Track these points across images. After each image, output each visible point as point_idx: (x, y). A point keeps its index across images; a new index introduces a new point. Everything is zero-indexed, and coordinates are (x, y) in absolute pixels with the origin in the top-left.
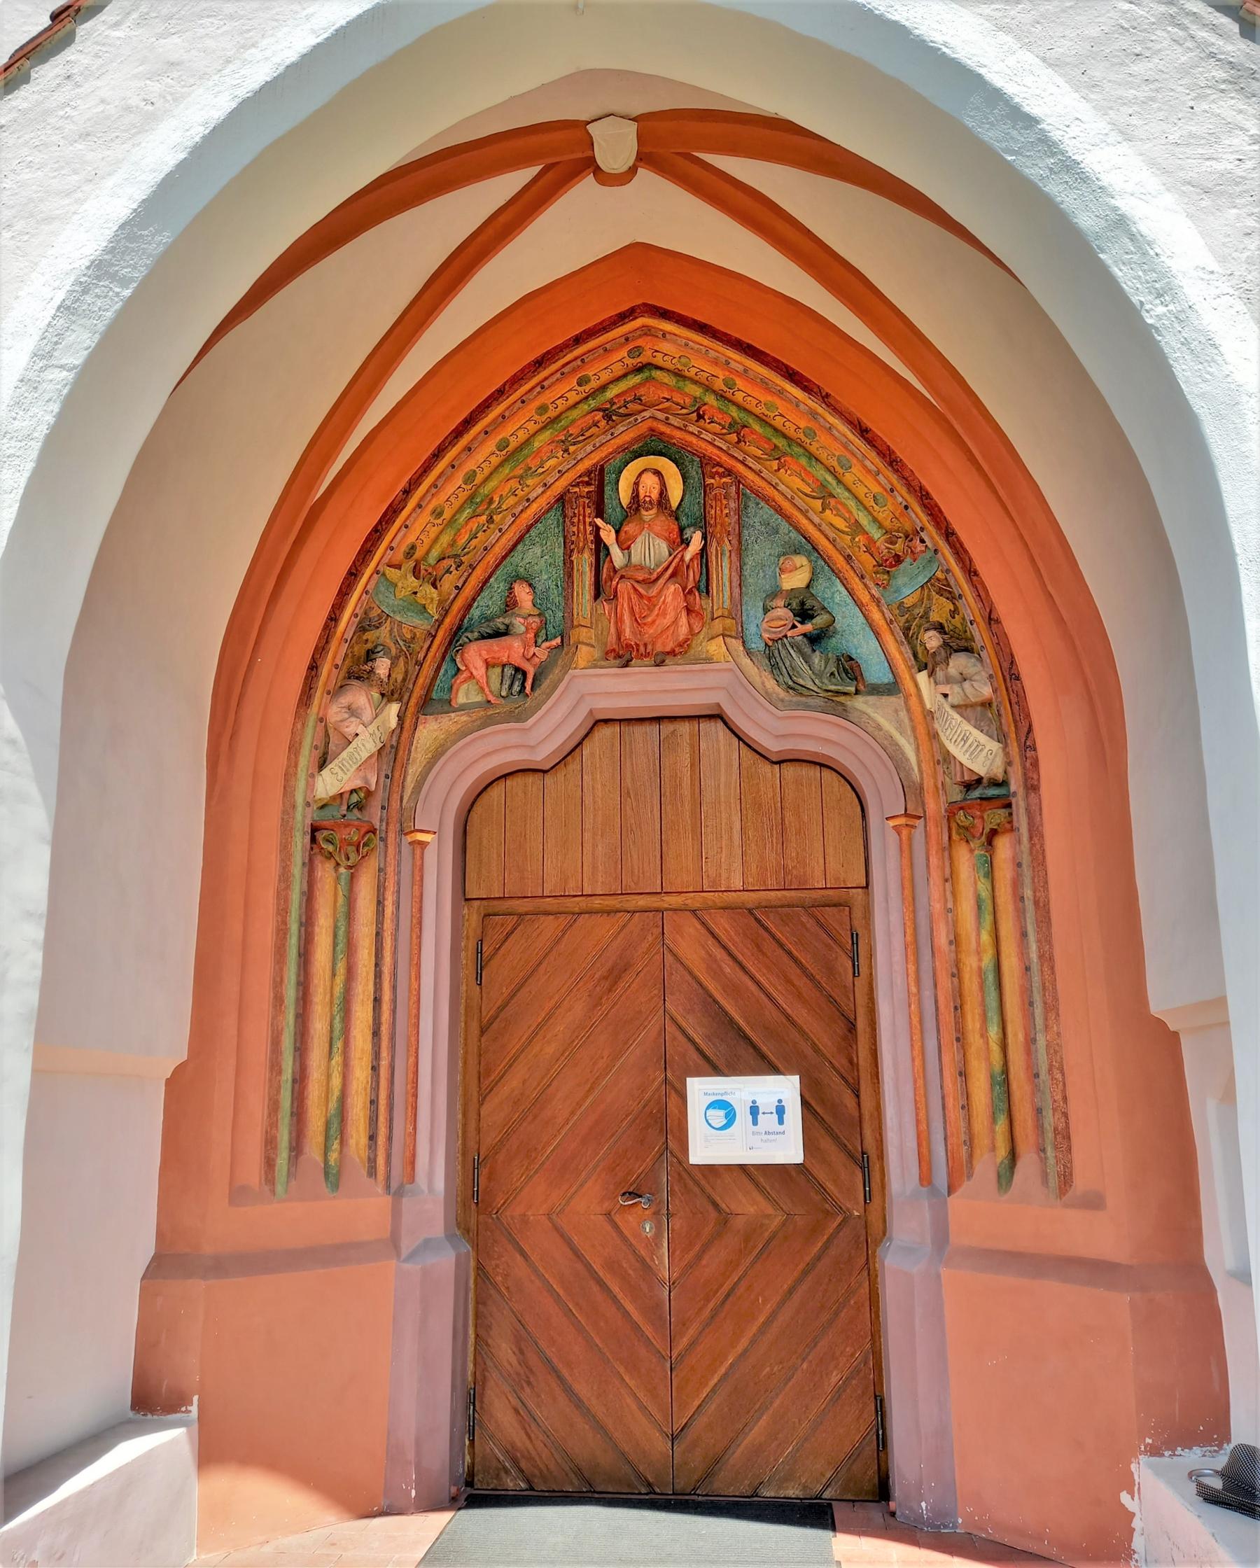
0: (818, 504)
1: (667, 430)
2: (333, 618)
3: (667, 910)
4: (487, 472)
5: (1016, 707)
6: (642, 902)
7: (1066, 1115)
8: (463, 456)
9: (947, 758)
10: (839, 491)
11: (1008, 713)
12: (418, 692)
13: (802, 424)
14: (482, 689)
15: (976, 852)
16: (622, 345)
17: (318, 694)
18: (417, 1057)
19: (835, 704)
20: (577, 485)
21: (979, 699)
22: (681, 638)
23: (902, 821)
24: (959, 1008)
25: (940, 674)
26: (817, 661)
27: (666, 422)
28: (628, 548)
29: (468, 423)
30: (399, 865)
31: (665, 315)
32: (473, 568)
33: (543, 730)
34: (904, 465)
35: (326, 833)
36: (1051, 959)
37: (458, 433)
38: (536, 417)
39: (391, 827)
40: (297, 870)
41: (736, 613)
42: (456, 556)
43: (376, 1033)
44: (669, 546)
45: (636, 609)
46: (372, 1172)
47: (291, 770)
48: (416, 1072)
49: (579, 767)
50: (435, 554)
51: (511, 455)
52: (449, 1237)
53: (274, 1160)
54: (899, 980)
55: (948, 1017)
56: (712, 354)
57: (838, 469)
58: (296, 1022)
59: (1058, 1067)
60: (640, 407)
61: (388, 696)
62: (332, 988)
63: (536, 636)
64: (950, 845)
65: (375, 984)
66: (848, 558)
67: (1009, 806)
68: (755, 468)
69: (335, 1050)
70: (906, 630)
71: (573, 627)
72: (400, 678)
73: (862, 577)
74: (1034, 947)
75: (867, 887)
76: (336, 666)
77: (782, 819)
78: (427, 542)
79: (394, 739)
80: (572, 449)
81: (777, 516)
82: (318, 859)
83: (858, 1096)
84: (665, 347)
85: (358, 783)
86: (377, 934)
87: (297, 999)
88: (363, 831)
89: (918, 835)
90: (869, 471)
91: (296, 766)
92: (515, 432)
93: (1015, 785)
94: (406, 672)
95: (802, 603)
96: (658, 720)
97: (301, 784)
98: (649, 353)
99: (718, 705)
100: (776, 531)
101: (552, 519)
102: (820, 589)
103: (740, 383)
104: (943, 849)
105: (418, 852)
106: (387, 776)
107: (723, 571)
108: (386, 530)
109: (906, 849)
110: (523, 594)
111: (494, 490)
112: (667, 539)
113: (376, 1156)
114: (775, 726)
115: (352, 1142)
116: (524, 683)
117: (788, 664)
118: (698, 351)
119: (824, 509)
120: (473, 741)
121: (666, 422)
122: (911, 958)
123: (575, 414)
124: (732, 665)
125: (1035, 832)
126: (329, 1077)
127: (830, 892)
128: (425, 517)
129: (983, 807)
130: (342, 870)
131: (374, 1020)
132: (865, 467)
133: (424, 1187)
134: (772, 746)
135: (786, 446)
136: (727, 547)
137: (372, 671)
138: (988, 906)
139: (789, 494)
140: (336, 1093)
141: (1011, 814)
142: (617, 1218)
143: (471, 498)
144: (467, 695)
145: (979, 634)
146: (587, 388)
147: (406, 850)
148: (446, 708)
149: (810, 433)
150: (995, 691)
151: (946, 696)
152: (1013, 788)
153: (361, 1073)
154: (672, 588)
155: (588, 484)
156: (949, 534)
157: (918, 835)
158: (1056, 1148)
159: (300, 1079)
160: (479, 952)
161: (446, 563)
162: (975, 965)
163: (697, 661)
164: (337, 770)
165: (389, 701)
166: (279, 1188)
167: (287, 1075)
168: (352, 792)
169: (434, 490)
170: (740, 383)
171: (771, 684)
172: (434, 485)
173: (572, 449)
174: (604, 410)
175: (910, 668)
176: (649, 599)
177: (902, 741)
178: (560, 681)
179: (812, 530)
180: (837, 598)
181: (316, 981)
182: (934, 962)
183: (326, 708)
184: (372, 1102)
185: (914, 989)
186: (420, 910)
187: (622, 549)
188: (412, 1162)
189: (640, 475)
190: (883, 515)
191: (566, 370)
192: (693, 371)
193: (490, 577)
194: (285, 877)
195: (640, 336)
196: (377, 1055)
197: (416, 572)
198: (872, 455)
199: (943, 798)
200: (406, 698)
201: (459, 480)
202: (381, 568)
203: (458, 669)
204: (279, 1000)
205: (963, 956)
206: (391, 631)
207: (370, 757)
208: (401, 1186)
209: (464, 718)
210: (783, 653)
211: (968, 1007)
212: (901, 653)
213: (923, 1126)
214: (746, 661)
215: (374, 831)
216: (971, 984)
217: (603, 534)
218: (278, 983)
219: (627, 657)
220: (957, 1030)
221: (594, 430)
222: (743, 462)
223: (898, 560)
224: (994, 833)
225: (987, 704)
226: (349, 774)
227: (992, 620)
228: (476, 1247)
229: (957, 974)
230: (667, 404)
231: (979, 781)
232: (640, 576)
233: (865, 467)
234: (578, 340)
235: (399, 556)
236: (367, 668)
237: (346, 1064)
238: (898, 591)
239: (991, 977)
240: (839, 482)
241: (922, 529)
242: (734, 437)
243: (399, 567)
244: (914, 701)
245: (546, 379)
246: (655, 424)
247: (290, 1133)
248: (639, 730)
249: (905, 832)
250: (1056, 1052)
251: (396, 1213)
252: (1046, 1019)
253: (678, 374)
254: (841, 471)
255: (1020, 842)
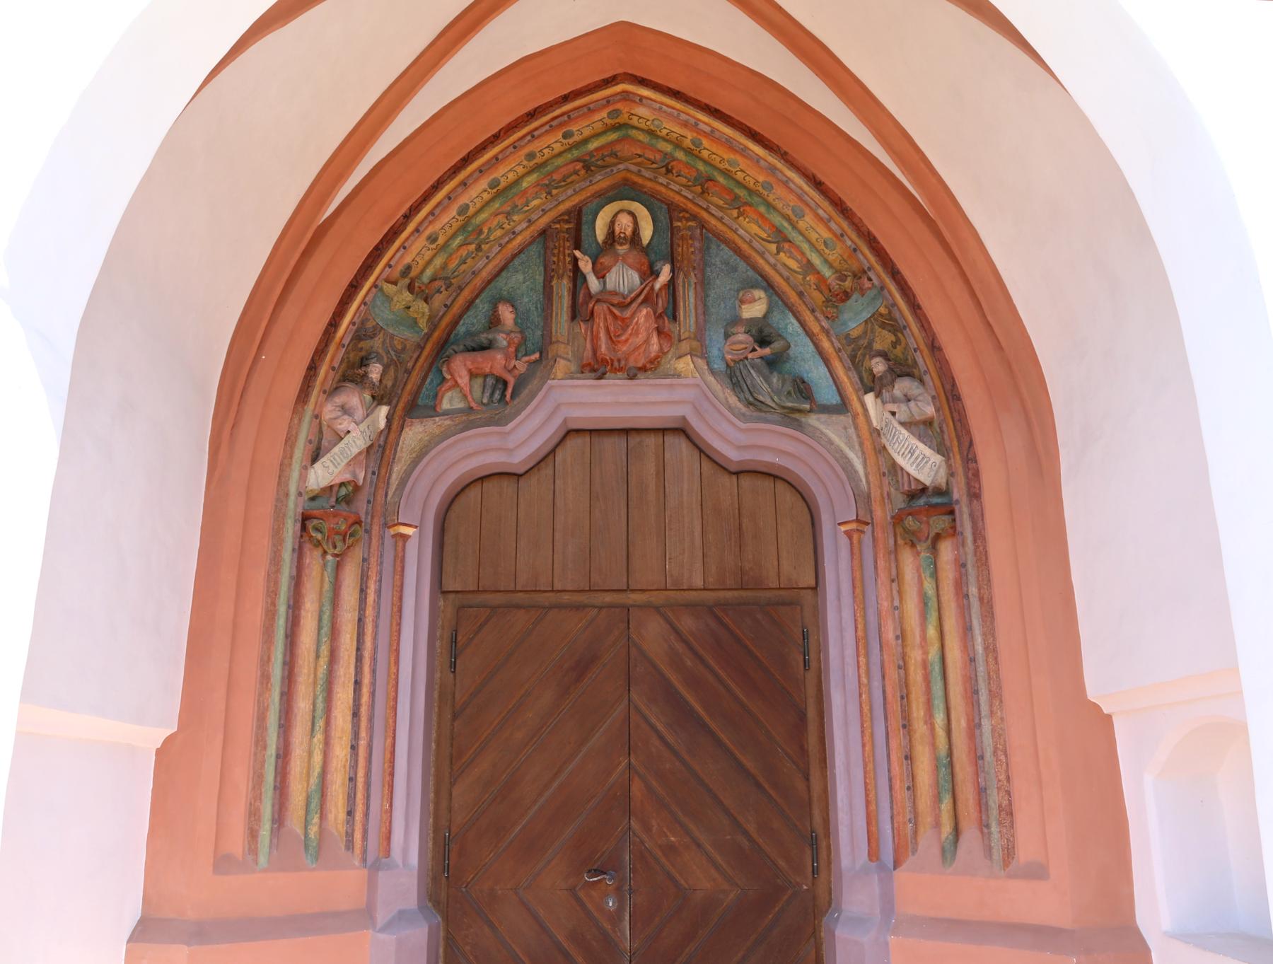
0: (773, 247)
1: (640, 181)
2: (334, 324)
3: (633, 606)
4: (478, 206)
5: (958, 425)
6: (608, 598)
7: (1008, 793)
8: (460, 190)
9: (895, 468)
10: (793, 235)
11: (950, 430)
12: (406, 397)
13: (761, 179)
14: (465, 396)
15: (922, 555)
16: (604, 107)
17: (315, 392)
18: (394, 738)
19: (791, 417)
20: (559, 222)
21: (923, 417)
22: (653, 355)
23: (853, 526)
24: (905, 697)
25: (886, 394)
26: (775, 380)
27: (639, 174)
28: (603, 277)
29: (466, 161)
30: (382, 556)
31: (643, 82)
32: (461, 289)
33: (522, 433)
34: (854, 214)
35: (315, 522)
36: (995, 650)
37: (456, 170)
38: (525, 163)
39: (376, 520)
40: (287, 555)
41: (700, 335)
42: (446, 278)
43: (356, 714)
44: (641, 277)
45: (612, 329)
46: (350, 844)
47: (286, 461)
48: (393, 753)
49: (551, 472)
50: (429, 273)
51: (500, 192)
52: (421, 907)
53: (257, 831)
54: (851, 671)
55: (895, 706)
56: (683, 117)
57: (792, 217)
58: (281, 699)
59: (1002, 750)
60: (616, 161)
61: (378, 399)
62: (316, 669)
63: (517, 350)
64: (896, 549)
65: (356, 667)
66: (801, 294)
67: (952, 512)
68: (716, 214)
69: (317, 728)
70: (853, 358)
71: (551, 343)
72: (389, 384)
73: (813, 311)
74: (979, 640)
75: (815, 589)
76: (333, 369)
77: (740, 525)
78: (421, 263)
79: (382, 439)
80: (554, 192)
81: (735, 257)
82: (307, 546)
83: (808, 780)
84: (641, 111)
85: (347, 477)
86: (360, 620)
87: (283, 678)
88: (351, 521)
89: (867, 539)
90: (821, 219)
91: (291, 458)
92: (505, 173)
93: (959, 493)
94: (396, 378)
95: (761, 331)
96: (626, 432)
97: (295, 475)
98: (626, 116)
99: (684, 418)
100: (735, 269)
101: (534, 250)
102: (776, 318)
103: (705, 143)
104: (890, 553)
105: (400, 544)
106: (374, 473)
107: (689, 300)
108: (387, 248)
109: (855, 553)
110: (506, 314)
111: (484, 222)
112: (639, 271)
113: (353, 830)
114: (734, 435)
115: (331, 817)
116: (505, 395)
117: (749, 382)
118: (670, 115)
119: (778, 253)
120: (456, 442)
121: (639, 174)
122: (862, 652)
123: (559, 161)
124: (699, 381)
125: (979, 535)
126: (310, 754)
127: (782, 593)
128: (421, 242)
129: (928, 514)
130: (329, 557)
131: (354, 701)
132: (817, 215)
133: (400, 862)
134: (733, 455)
135: (743, 199)
136: (693, 280)
137: (365, 375)
138: (933, 604)
139: (747, 237)
140: (317, 770)
141: (954, 520)
142: (581, 894)
143: (463, 228)
144: (451, 400)
145: (923, 361)
146: (571, 141)
147: (388, 542)
148: (432, 413)
149: (769, 186)
150: (937, 410)
151: (893, 414)
152: (956, 496)
153: (341, 752)
154: (644, 312)
155: (568, 222)
156: (895, 274)
157: (867, 539)
158: (1000, 823)
159: (284, 755)
160: (454, 641)
161: (437, 284)
162: (919, 658)
163: (666, 376)
164: (328, 463)
165: (380, 403)
166: (263, 860)
167: (272, 751)
168: (342, 484)
169: (431, 218)
170: (705, 143)
171: (733, 400)
172: (431, 213)
173: (554, 192)
174: (584, 161)
175: (857, 391)
176: (623, 320)
177: (851, 455)
178: (539, 390)
179: (767, 268)
180: (790, 329)
181: (300, 662)
182: (882, 655)
183: (321, 406)
184: (351, 779)
185: (864, 680)
186: (401, 598)
187: (598, 278)
188: (388, 837)
189: (616, 215)
190: (833, 256)
191: (554, 123)
192: (665, 132)
193: (477, 296)
194: (276, 560)
195: (619, 101)
196: (356, 735)
197: (411, 288)
198: (825, 204)
199: (888, 507)
200: (394, 402)
201: (453, 212)
202: (379, 283)
203: (444, 378)
204: (265, 677)
205: (908, 649)
206: (383, 343)
207: (360, 453)
208: (377, 860)
209: (448, 422)
210: (744, 372)
211: (913, 696)
212: (849, 378)
213: (873, 807)
214: (711, 379)
215: (359, 522)
216: (916, 676)
217: (581, 264)
218: (265, 661)
219: (602, 370)
220: (904, 718)
221: (574, 177)
222: (706, 210)
223: (846, 296)
224: (938, 537)
225: (928, 423)
226: (340, 468)
227: (934, 347)
228: (446, 919)
229: (904, 667)
230: (639, 160)
231: (924, 490)
232: (616, 300)
233: (817, 215)
234: (566, 99)
235: (396, 273)
236: (361, 371)
237: (327, 743)
238: (844, 324)
239: (937, 668)
240: (794, 227)
241: (869, 269)
242: (699, 189)
243: (395, 283)
244: (861, 419)
245: (536, 129)
246: (629, 175)
247: (273, 806)
248: (608, 443)
249: (855, 537)
250: (1000, 735)
251: (372, 884)
252: (991, 706)
253: (651, 132)
254: (795, 219)
255: (963, 544)
